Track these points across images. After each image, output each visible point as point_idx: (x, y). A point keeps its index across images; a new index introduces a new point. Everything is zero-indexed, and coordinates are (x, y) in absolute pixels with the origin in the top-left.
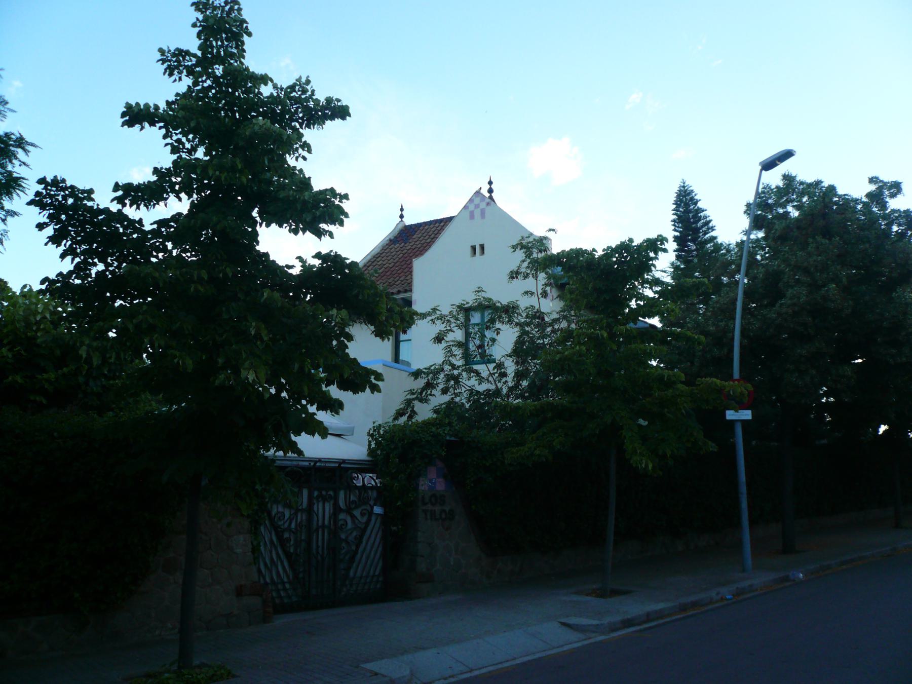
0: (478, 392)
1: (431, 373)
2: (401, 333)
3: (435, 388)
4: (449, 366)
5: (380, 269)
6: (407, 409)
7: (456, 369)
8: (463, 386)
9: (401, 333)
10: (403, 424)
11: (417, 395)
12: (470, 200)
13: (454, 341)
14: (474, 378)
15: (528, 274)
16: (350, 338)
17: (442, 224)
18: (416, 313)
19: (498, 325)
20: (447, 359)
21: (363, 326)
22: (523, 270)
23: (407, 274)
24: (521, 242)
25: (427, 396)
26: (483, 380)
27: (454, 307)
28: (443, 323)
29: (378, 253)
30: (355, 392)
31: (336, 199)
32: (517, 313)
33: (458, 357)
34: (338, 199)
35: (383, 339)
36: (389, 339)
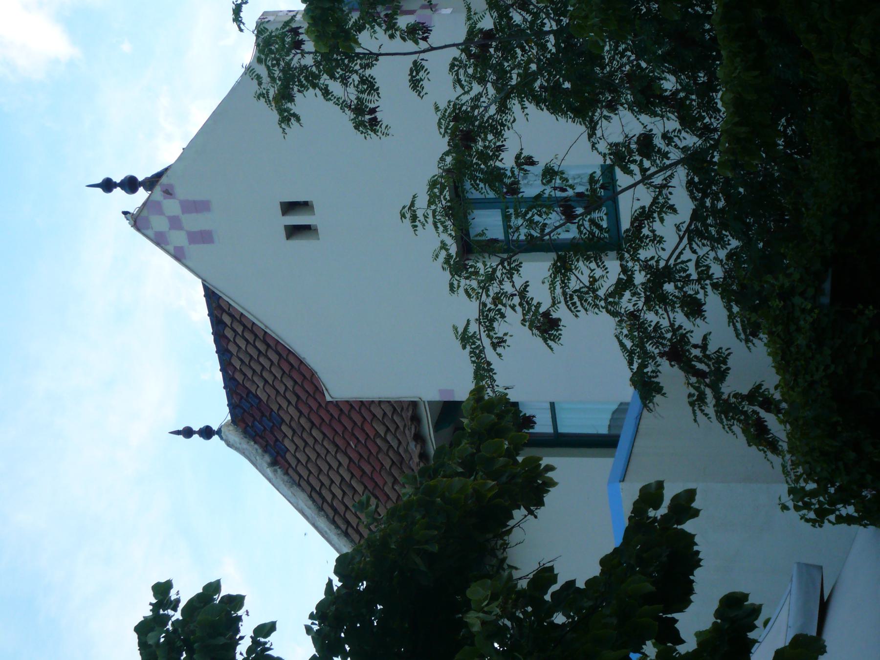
0: (695, 216)
1: (641, 345)
2: (531, 431)
3: (684, 336)
4: (621, 296)
6: (745, 413)
8: (678, 257)
10: (788, 427)
11: (707, 385)
12: (158, 244)
13: (553, 284)
14: (657, 225)
15: (363, 80)
16: (545, 575)
17: (226, 319)
18: (478, 392)
19: (507, 161)
20: (602, 303)
21: (515, 536)
22: (352, 94)
25: (708, 357)
26: (661, 200)
28: (503, 316)
29: (310, 497)
30: (694, 561)
31: (169, 617)
32: (474, 108)
33: (598, 273)
34: (170, 612)
35: (552, 483)
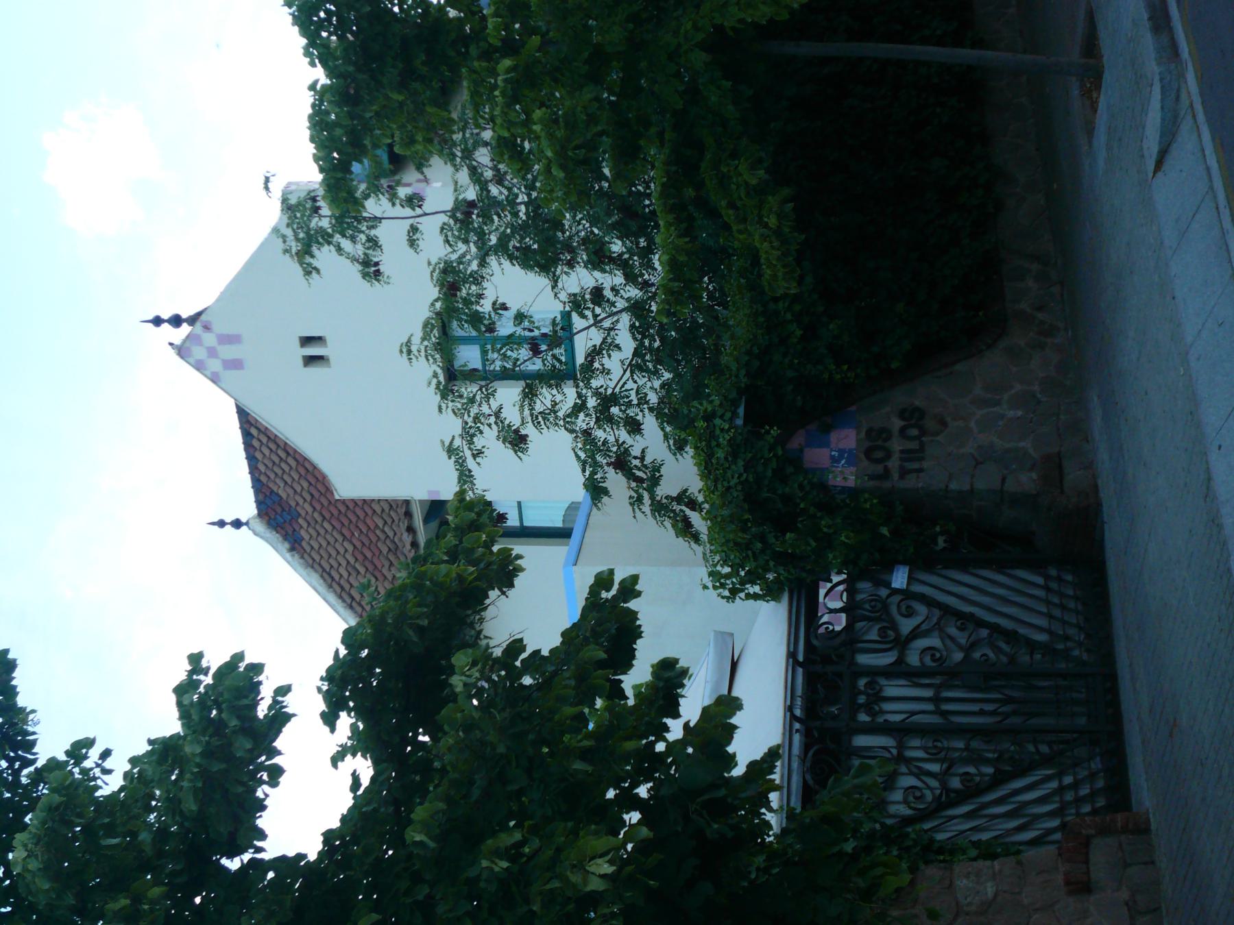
0: (636, 353)
4: (577, 417)
7: (584, 403)
8: (623, 386)
13: (522, 406)
14: (605, 360)
15: (370, 239)
16: (516, 646)
17: (254, 432)
18: (461, 494)
19: (486, 307)
20: (562, 423)
22: (359, 250)
23: (370, 512)
24: (297, 254)
27: (444, 406)
28: (481, 432)
29: (322, 576)
31: (200, 682)
33: (559, 398)
34: (202, 677)
36: (519, 557)
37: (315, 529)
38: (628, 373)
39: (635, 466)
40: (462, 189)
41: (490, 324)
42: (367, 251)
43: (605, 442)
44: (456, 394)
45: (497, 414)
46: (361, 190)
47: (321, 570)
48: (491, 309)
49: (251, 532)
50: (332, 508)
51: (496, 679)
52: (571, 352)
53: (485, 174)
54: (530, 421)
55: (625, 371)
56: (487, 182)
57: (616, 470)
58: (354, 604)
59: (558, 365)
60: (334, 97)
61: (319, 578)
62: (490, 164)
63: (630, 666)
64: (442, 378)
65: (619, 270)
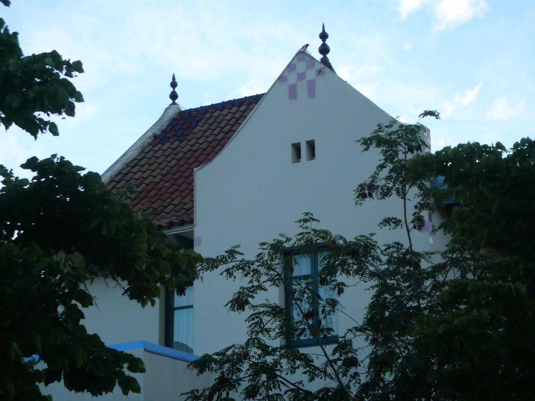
0: (308, 393)
2: (176, 293)
3: (234, 386)
4: (258, 348)
5: (138, 186)
7: (269, 354)
8: (282, 383)
9: (176, 293)
12: (289, 66)
13: (266, 306)
14: (302, 370)
15: (389, 189)
16: (87, 300)
17: (243, 108)
18: (199, 258)
19: (341, 277)
20: (254, 337)
21: (112, 283)
22: (381, 183)
23: (183, 194)
24: (378, 135)
27: (265, 247)
28: (246, 275)
29: (135, 159)
31: (61, 70)
33: (273, 334)
34: (64, 72)
36: (153, 303)
37: (171, 153)
38: (292, 387)
39: (221, 394)
40: (428, 258)
41: (327, 281)
42: (380, 188)
43: (240, 370)
44: (274, 256)
45: (260, 287)
46: (425, 183)
47: (139, 158)
48: (338, 282)
49: (168, 106)
50: (186, 166)
51: (62, 286)
52: (307, 344)
53: (440, 276)
54: (255, 312)
55: (293, 385)
56: (434, 277)
57: (218, 378)
58: (114, 183)
59: (298, 333)
60: (492, 161)
61: (134, 157)
62: (448, 279)
63: (70, 389)
64: (286, 245)
65: (370, 379)
